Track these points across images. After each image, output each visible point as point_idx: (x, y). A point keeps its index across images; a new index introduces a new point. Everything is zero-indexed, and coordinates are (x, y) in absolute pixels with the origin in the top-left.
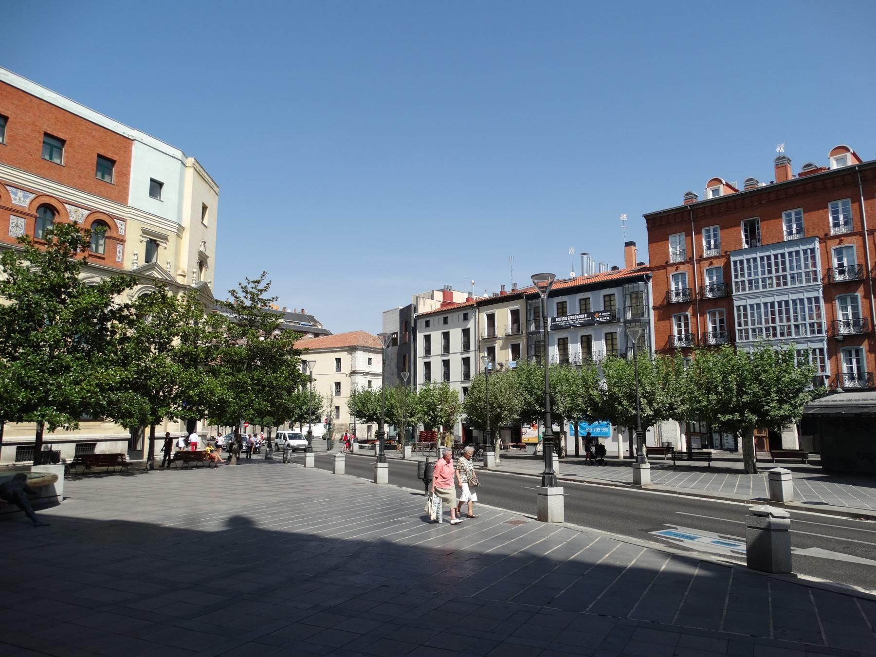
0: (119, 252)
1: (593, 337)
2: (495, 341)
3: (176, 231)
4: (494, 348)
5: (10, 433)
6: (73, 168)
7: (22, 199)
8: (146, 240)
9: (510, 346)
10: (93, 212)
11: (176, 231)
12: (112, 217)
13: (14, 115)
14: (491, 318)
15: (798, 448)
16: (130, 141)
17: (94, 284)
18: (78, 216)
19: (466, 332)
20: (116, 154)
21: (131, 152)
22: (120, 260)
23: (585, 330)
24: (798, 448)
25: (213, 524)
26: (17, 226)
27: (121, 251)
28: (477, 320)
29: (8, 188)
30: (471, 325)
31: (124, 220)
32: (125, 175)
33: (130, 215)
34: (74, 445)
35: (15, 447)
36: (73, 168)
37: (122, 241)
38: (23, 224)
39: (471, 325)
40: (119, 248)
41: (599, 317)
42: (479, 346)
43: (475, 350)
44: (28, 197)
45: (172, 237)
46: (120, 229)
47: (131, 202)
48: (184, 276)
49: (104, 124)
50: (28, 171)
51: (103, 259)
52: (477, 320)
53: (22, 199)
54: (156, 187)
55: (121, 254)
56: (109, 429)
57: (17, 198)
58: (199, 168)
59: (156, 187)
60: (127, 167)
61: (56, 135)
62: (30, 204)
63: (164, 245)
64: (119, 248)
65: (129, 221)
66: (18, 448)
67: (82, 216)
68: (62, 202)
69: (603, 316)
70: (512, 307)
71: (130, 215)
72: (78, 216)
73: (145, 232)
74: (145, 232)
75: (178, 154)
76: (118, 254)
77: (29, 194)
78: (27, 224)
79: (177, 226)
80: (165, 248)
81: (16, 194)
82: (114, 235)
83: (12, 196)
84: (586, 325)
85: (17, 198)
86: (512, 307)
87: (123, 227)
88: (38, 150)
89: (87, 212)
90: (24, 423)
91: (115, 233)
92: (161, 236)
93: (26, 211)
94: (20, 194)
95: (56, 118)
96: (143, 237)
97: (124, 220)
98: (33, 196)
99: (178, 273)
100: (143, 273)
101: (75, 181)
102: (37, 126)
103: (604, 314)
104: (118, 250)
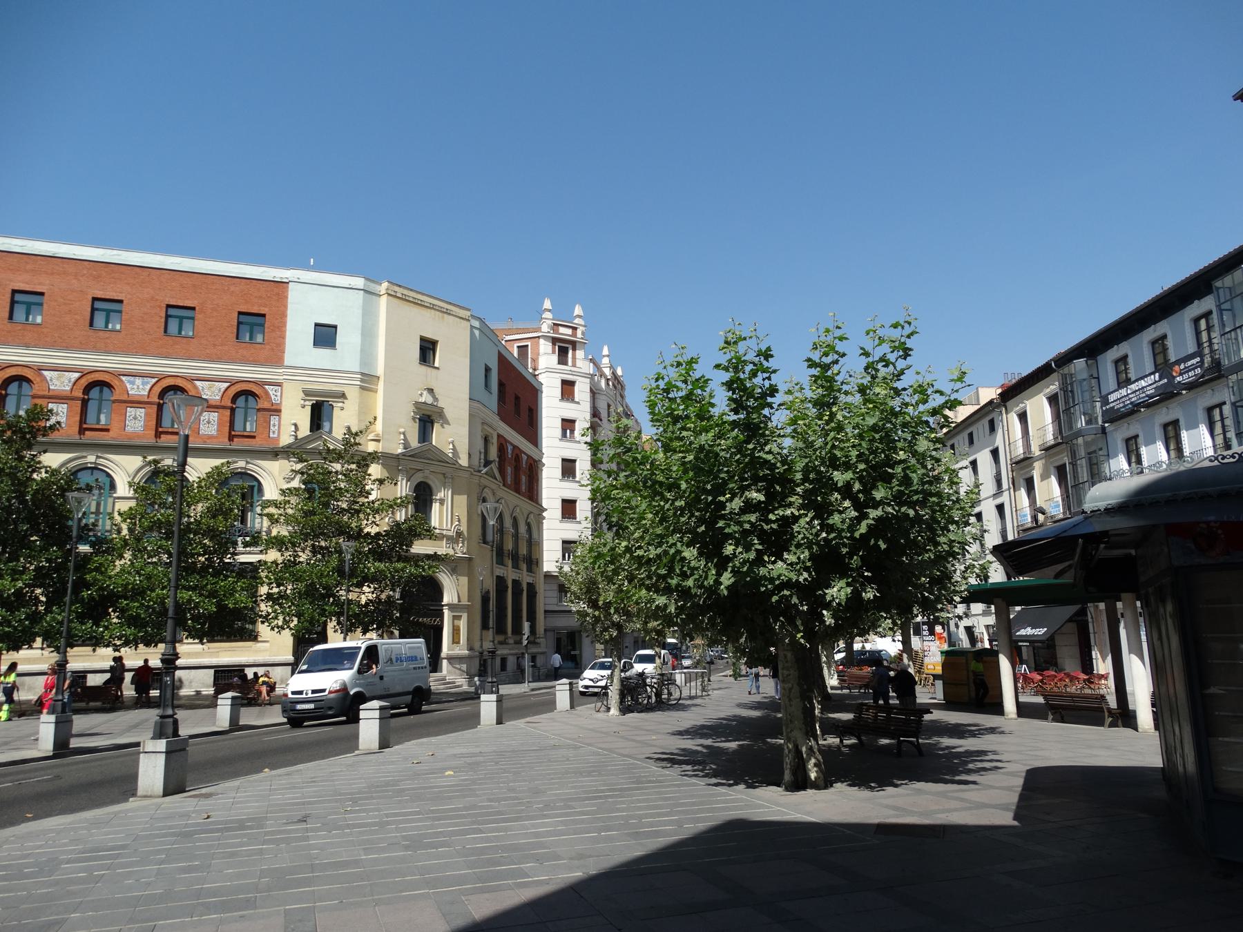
0: (274, 426)
1: (1182, 423)
2: (1032, 464)
3: (359, 383)
4: (1032, 478)
5: (189, 655)
6: (204, 337)
7: (141, 387)
8: (310, 403)
9: (1053, 470)
10: (233, 383)
11: (359, 383)
12: (261, 384)
13: (129, 296)
14: (1023, 417)
15: (71, 746)
16: (285, 285)
17: (239, 470)
18: (213, 392)
19: (995, 453)
20: (265, 306)
21: (287, 297)
22: (276, 436)
23: (1164, 410)
24: (71, 746)
25: (742, 787)
26: (135, 418)
27: (277, 423)
28: (1006, 428)
29: (124, 378)
30: (999, 441)
31: (279, 385)
32: (281, 328)
33: (285, 377)
34: (212, 671)
35: (212, 671)
36: (204, 337)
37: (277, 411)
38: (143, 415)
39: (999, 441)
40: (274, 420)
41: (1181, 374)
42: (1013, 478)
43: (1009, 489)
44: (148, 383)
45: (353, 394)
46: (273, 397)
47: (288, 360)
48: (378, 441)
49: (245, 274)
50: (146, 354)
51: (254, 437)
52: (1006, 428)
53: (141, 387)
54: (325, 336)
55: (276, 428)
56: (260, 651)
57: (135, 387)
58: (400, 291)
59: (325, 336)
60: (281, 318)
61: (181, 304)
62: (150, 390)
63: (340, 405)
64: (274, 420)
65: (285, 385)
66: (216, 672)
67: (220, 391)
68: (192, 380)
69: (1188, 370)
70: (1048, 390)
71: (285, 377)
72: (213, 392)
73: (307, 393)
74: (307, 393)
75: (359, 282)
76: (272, 428)
77: (149, 379)
78: (146, 414)
79: (359, 376)
80: (342, 409)
81: (133, 383)
82: (266, 405)
83: (129, 386)
84: (1167, 395)
85: (135, 387)
86: (1048, 390)
87: (279, 394)
88: (158, 328)
89: (77, 375)
90: (75, 649)
91: (266, 403)
92: (327, 394)
93: (146, 399)
94: (138, 381)
95: (181, 285)
96: (305, 400)
97: (279, 385)
98: (154, 380)
99: (369, 438)
100: (304, 446)
101: (208, 351)
102: (157, 300)
103: (1190, 363)
104: (272, 423)
